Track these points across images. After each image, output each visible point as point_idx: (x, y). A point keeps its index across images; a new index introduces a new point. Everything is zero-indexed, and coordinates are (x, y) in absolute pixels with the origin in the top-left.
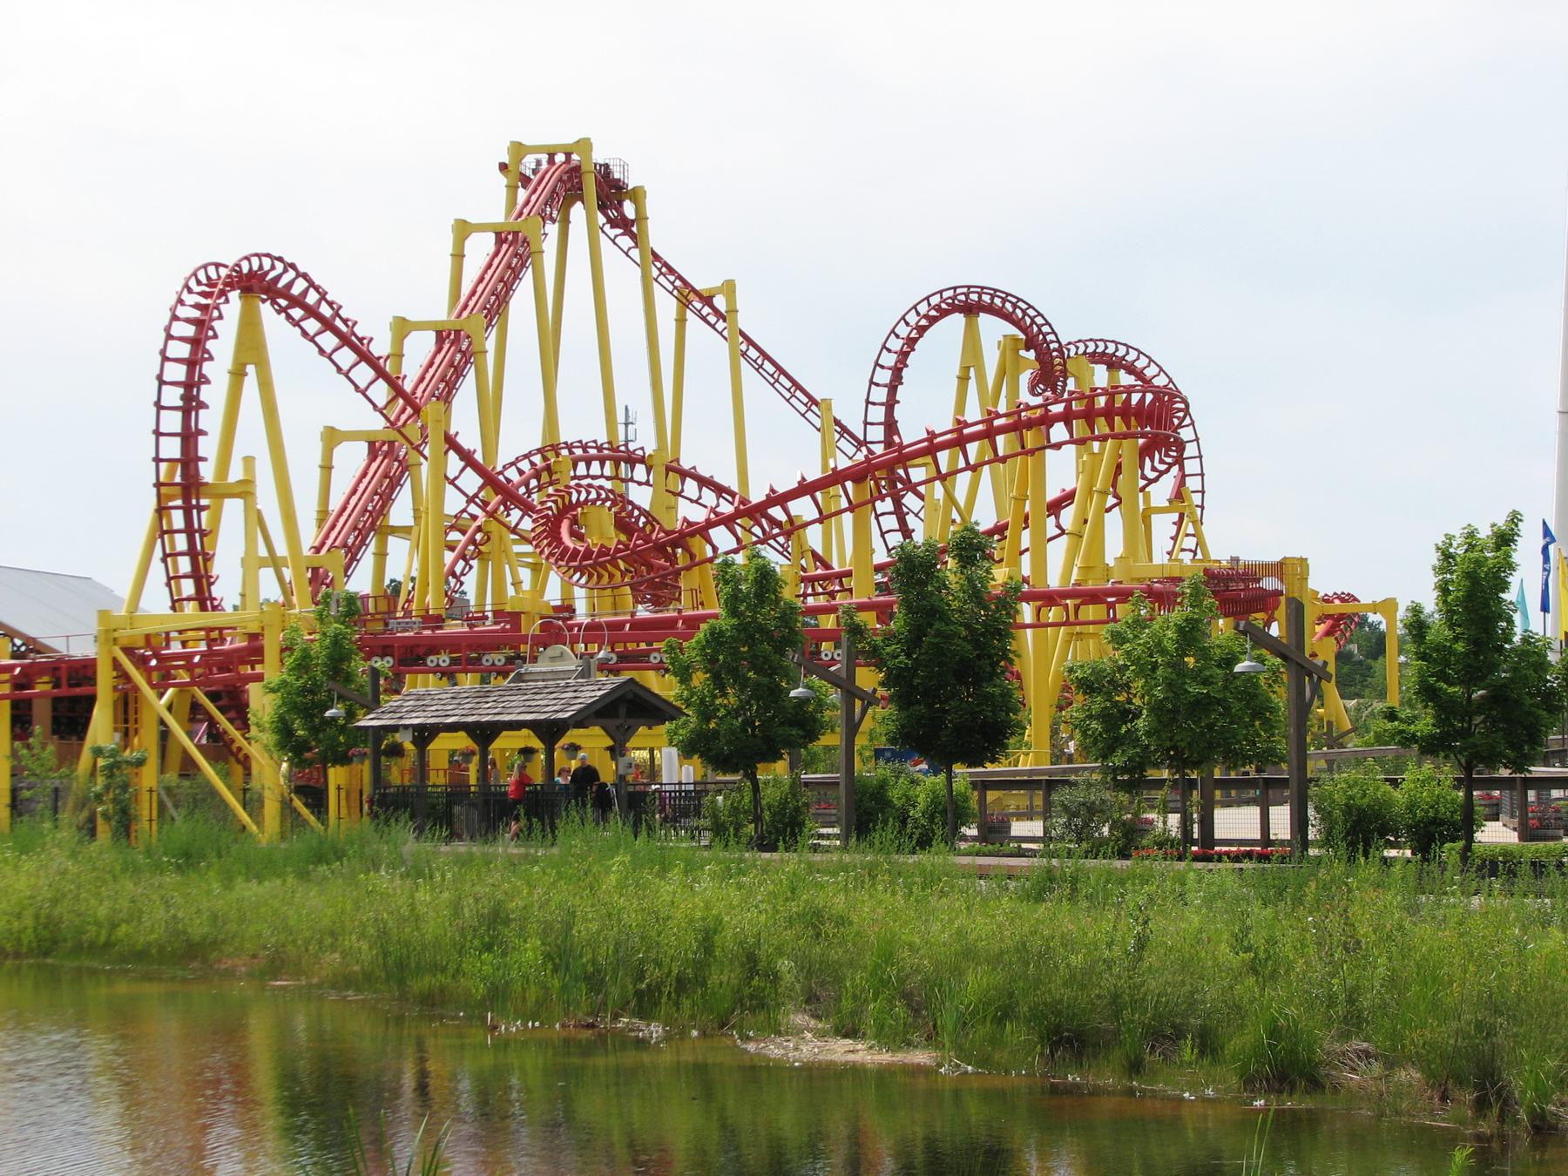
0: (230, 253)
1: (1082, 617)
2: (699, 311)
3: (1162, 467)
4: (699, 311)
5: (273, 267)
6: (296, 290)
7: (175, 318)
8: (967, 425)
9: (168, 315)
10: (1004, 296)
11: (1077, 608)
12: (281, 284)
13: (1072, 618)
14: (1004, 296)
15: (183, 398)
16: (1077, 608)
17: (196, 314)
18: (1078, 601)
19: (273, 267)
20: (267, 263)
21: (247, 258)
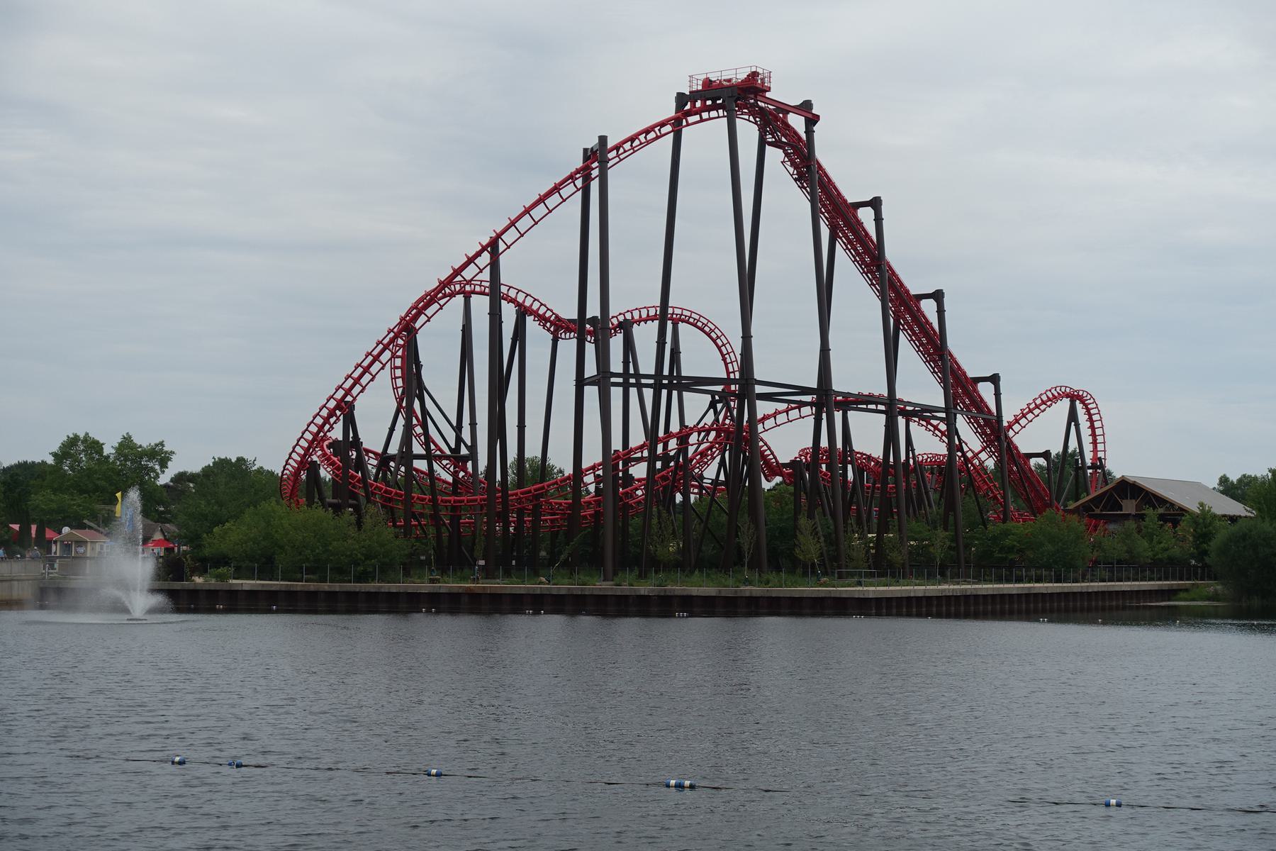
0: (1077, 385)
1: (662, 133)
2: (641, 143)
3: (285, 472)
4: (641, 143)
5: (1086, 396)
6: (547, 315)
7: (1050, 391)
8: (1017, 416)
9: (1050, 388)
10: (635, 149)
11: (659, 130)
12: (299, 459)
13: (659, 134)
14: (635, 149)
15: (1067, 398)
16: (659, 130)
17: (1056, 394)
18: (659, 128)
19: (1086, 396)
20: (1089, 397)
21: (1083, 391)
